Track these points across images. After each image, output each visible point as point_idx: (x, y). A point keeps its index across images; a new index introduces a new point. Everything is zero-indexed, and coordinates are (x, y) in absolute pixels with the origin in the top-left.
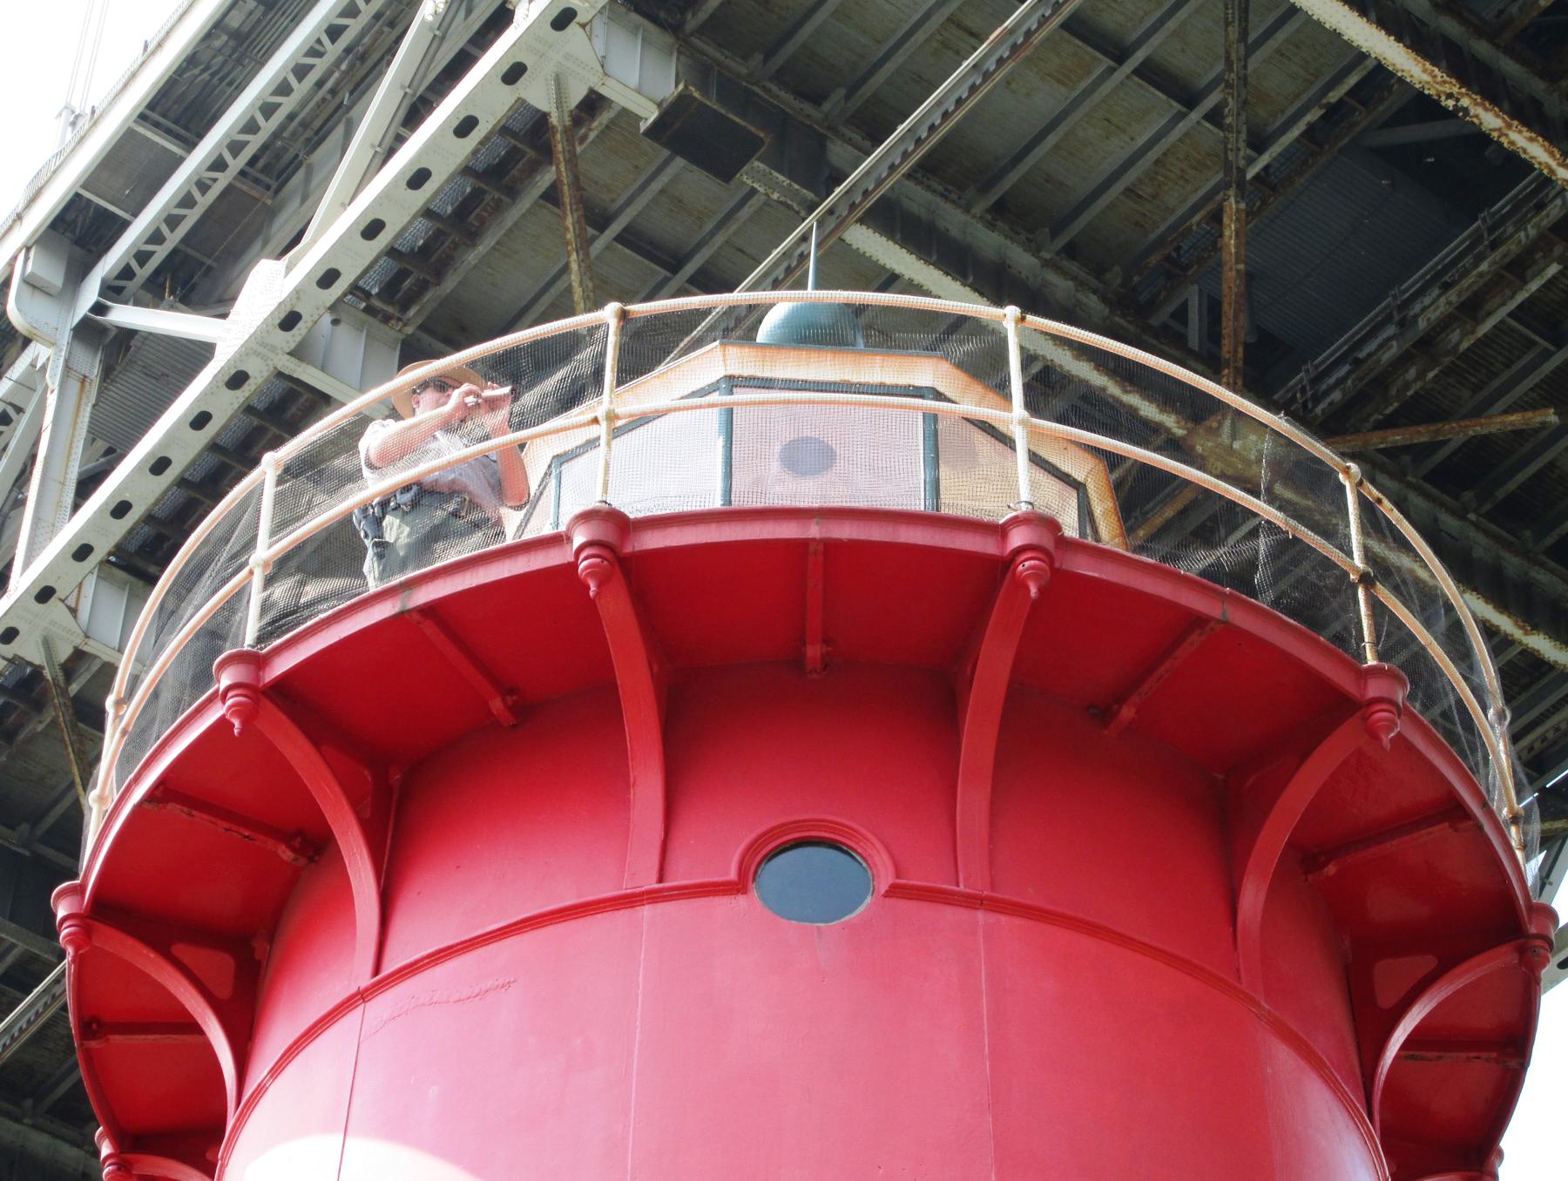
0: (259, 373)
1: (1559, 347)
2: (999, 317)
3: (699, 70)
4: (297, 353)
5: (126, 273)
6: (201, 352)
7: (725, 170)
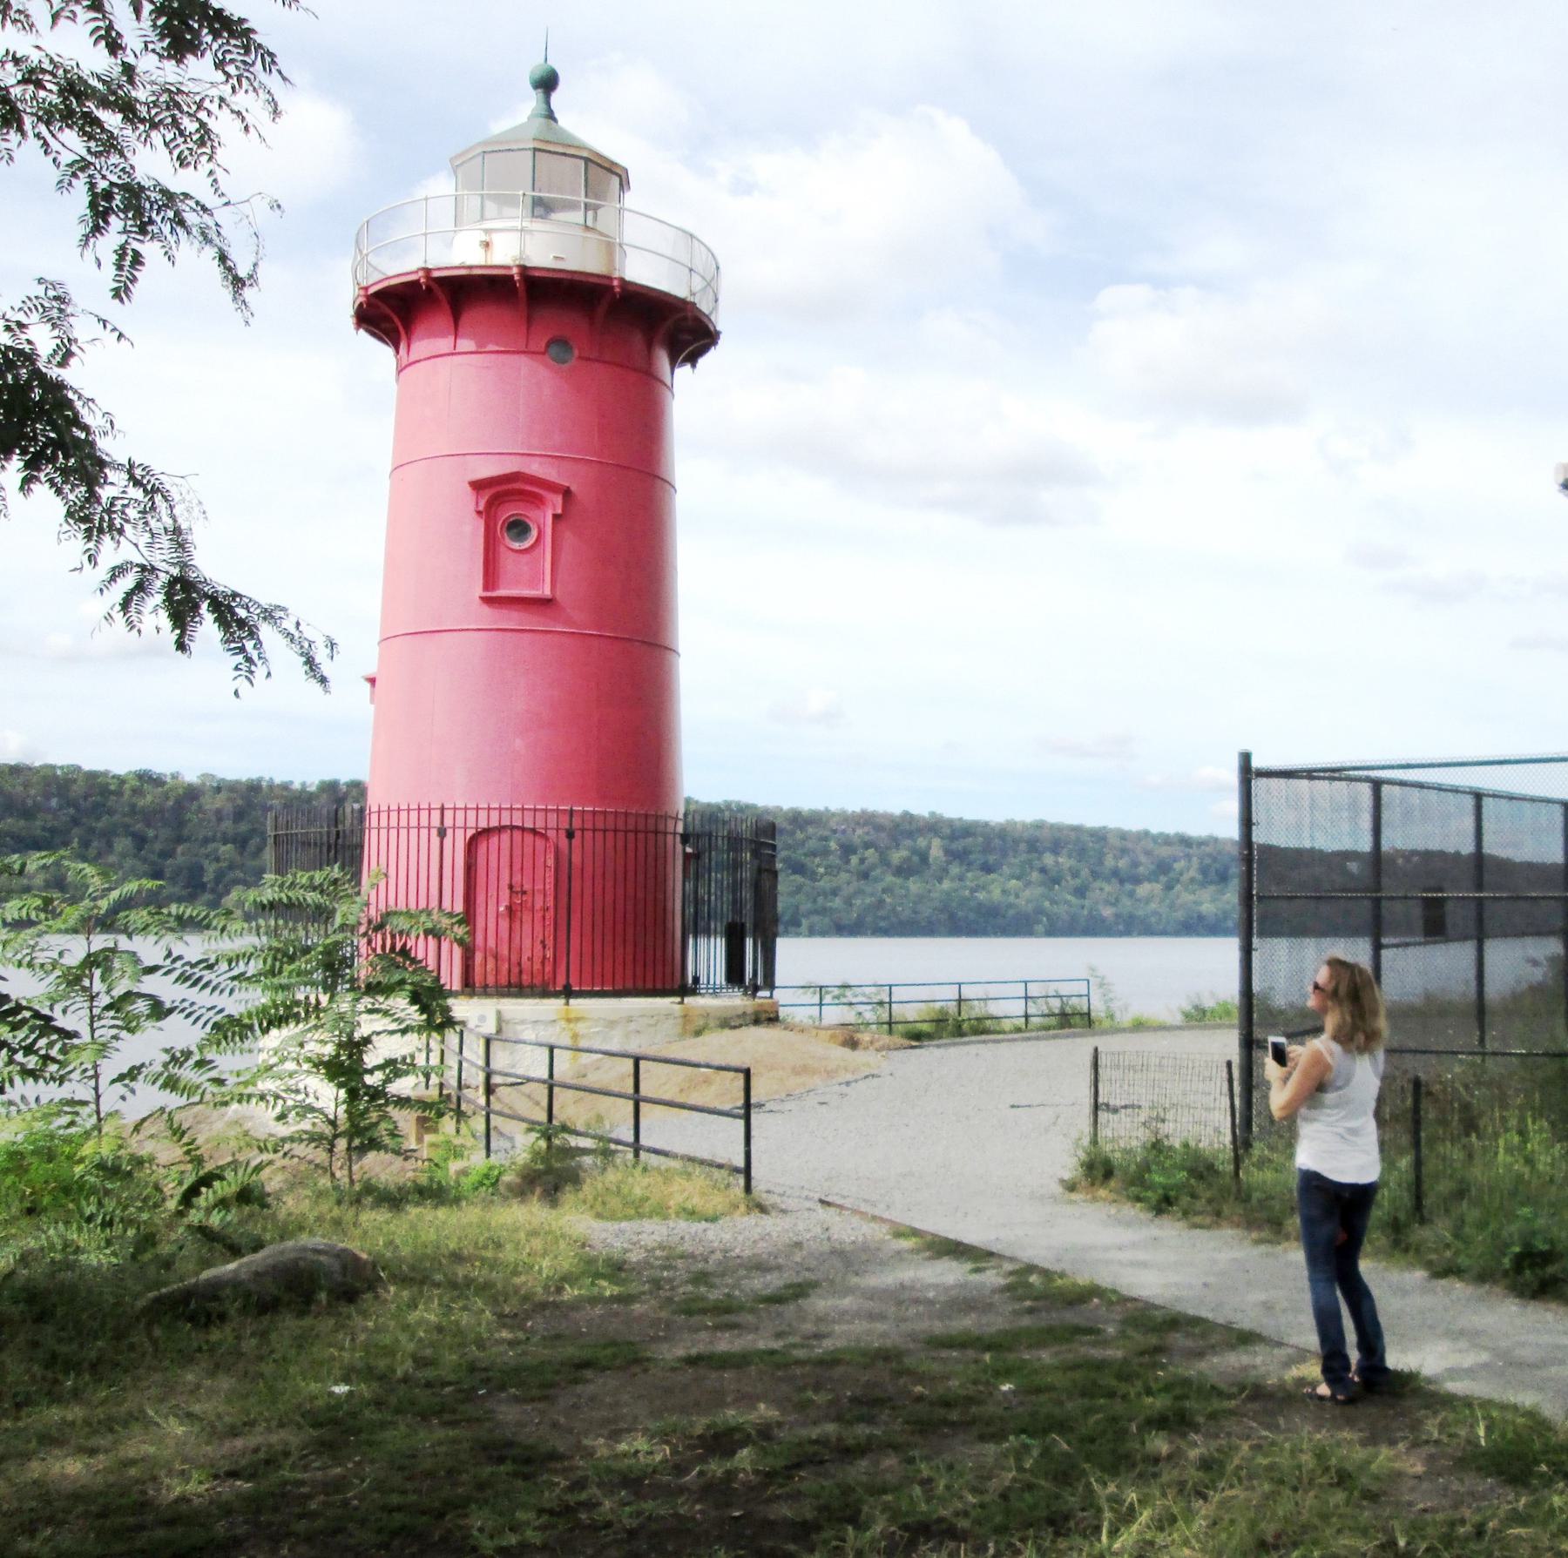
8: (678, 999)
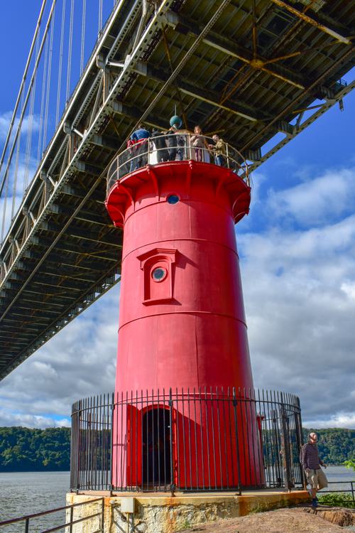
0: (129, 72)
1: (2, 321)
2: (147, 163)
3: (181, 19)
4: (134, 68)
5: (111, 57)
6: (121, 69)
7: (186, 34)
8: (238, 493)
